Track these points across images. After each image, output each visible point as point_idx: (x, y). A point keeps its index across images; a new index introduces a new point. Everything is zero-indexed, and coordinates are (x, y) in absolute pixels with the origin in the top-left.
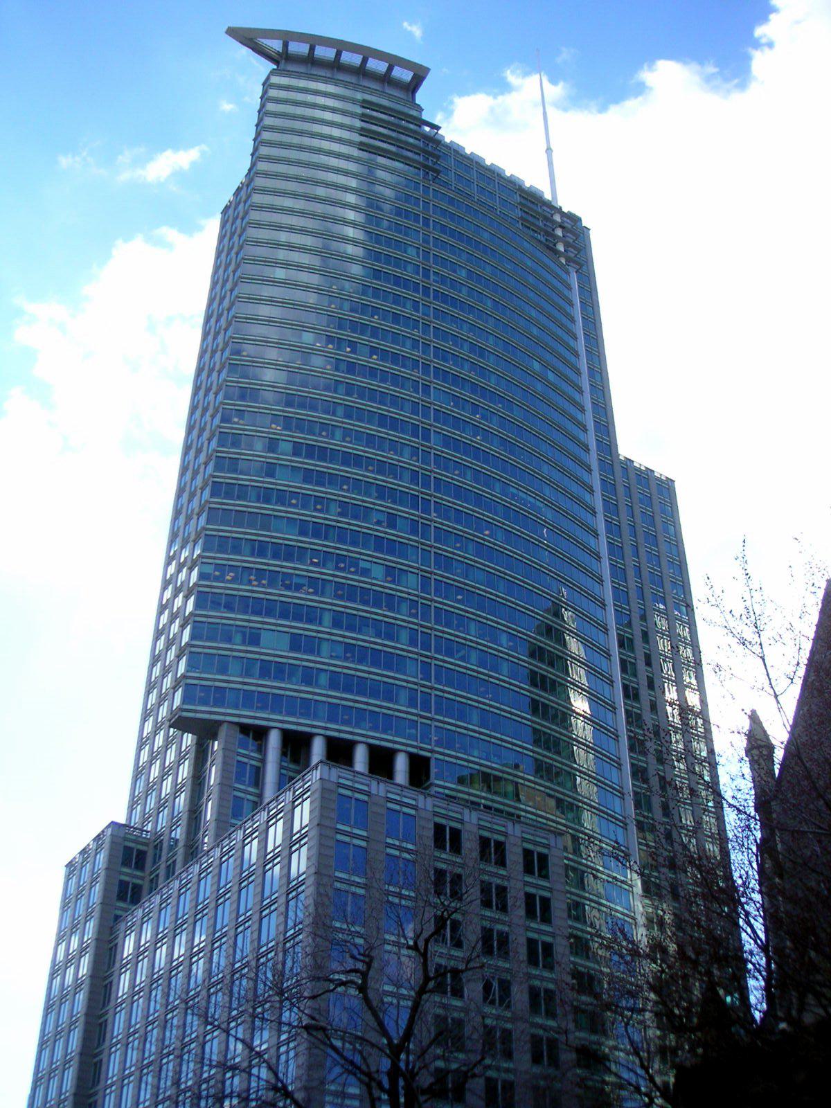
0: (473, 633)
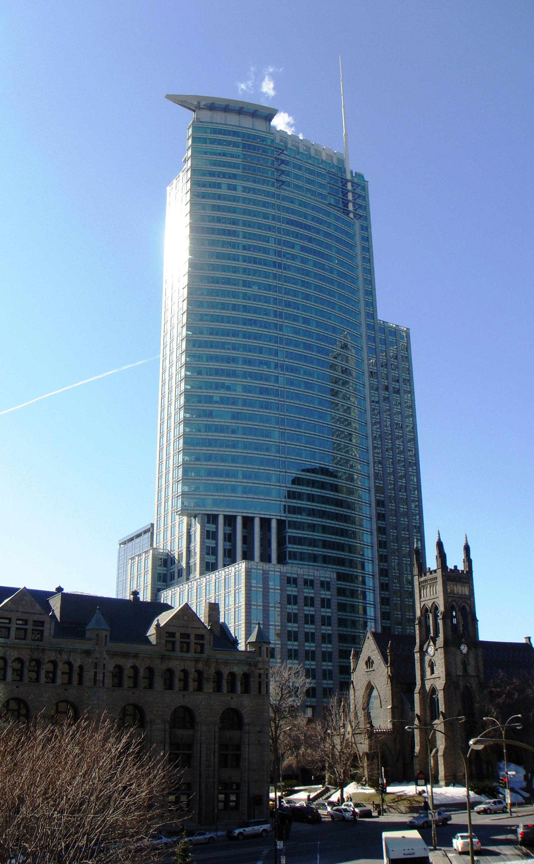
0: (303, 438)
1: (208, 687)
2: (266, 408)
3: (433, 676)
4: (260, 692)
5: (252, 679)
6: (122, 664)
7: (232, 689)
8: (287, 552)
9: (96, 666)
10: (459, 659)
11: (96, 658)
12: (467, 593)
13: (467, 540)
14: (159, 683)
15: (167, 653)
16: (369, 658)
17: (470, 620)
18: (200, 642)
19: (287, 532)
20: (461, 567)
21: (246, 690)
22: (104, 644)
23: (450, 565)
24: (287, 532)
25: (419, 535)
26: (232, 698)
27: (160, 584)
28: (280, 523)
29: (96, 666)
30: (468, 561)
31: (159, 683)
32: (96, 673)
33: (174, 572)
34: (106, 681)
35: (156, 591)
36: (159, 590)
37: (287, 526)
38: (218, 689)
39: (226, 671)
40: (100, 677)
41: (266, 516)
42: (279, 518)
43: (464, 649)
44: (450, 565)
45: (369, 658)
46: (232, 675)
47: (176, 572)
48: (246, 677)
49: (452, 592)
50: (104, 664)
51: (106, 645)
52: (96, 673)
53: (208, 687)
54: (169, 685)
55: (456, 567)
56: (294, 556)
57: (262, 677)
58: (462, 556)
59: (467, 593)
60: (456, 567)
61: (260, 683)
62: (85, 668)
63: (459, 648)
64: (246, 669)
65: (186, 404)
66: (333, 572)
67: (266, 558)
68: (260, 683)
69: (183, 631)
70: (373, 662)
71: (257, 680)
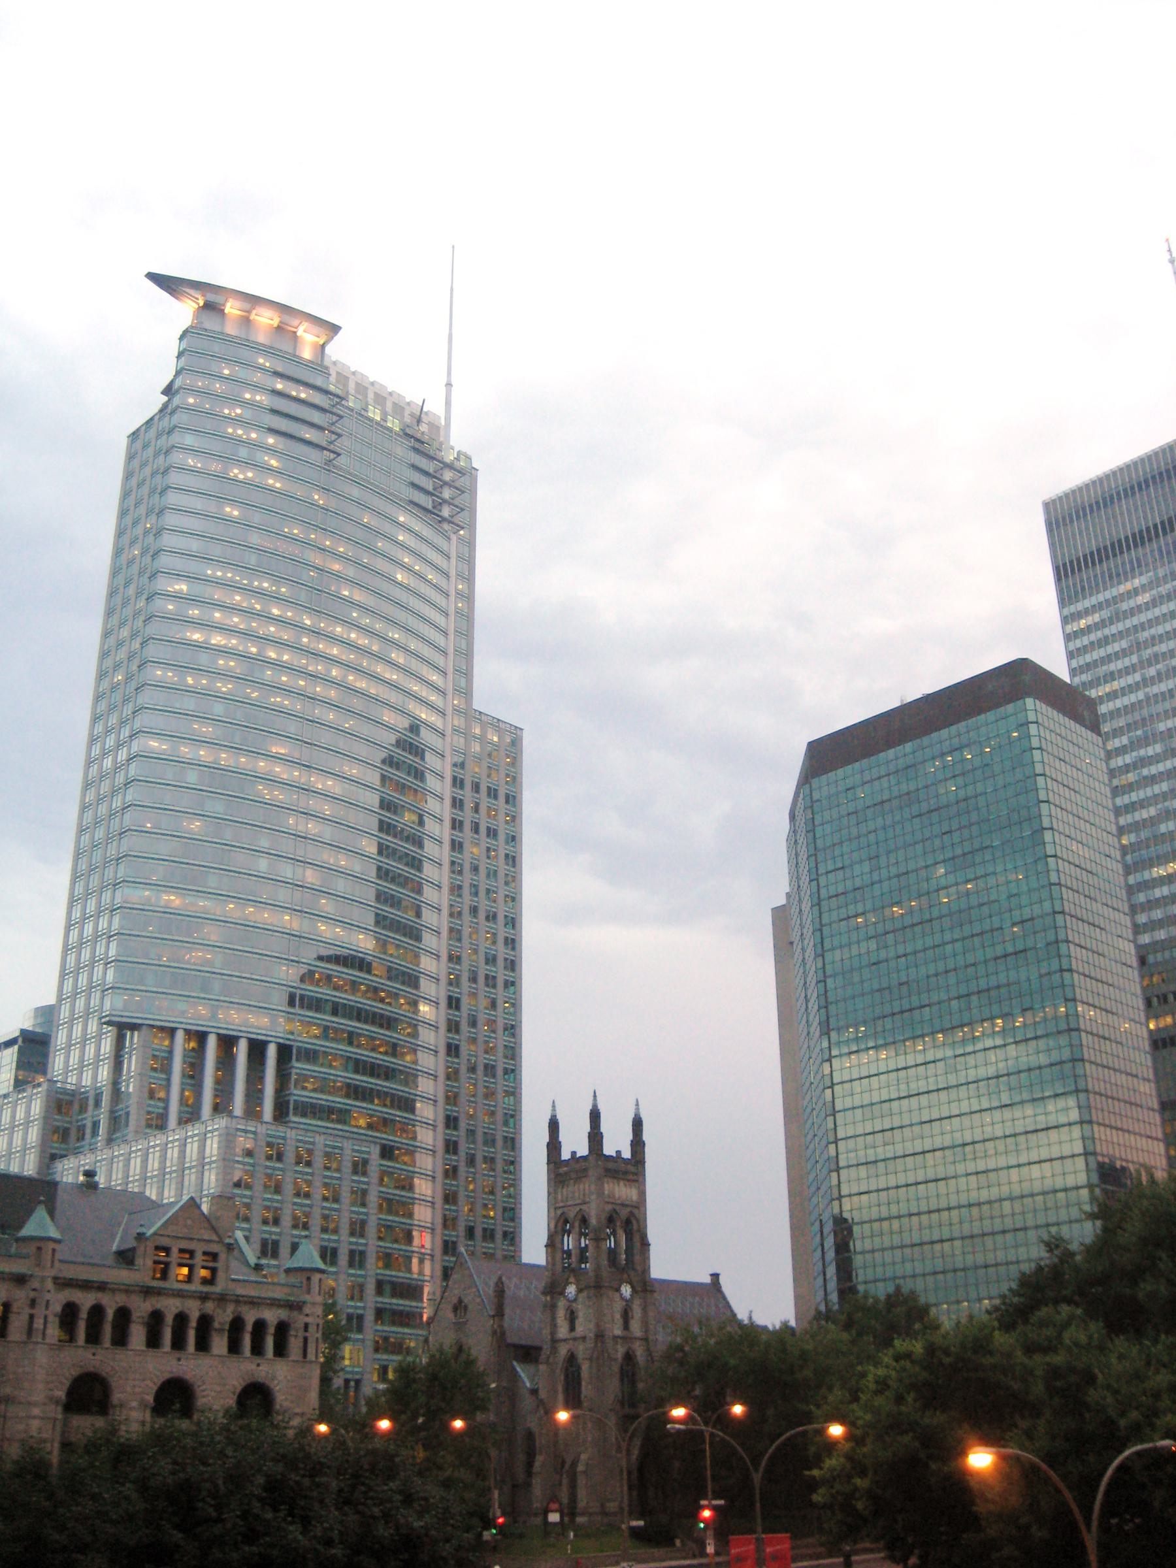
1: (219, 1344)
2: (389, 810)
3: (573, 1334)
4: (305, 1355)
5: (292, 1333)
6: (77, 1301)
7: (257, 1350)
8: (292, 1103)
9: (33, 1303)
10: (618, 1306)
11: (34, 1290)
12: (635, 1198)
13: (637, 1109)
14: (138, 1334)
15: (155, 1284)
16: (460, 1301)
17: (637, 1245)
18: (211, 1264)
19: (292, 1067)
20: (627, 1154)
21: (281, 1350)
22: (49, 1265)
23: (609, 1149)
24: (292, 1067)
25: (164, 1076)
26: (258, 1365)
27: (56, 1147)
28: (284, 1052)
29: (33, 1303)
30: (638, 1143)
31: (138, 1334)
32: (32, 1317)
33: (84, 1126)
34: (49, 1331)
35: (50, 1158)
36: (53, 1157)
37: (294, 1057)
38: (234, 1347)
39: (250, 1317)
40: (38, 1324)
41: (260, 1037)
42: (281, 1041)
43: (626, 1290)
44: (609, 1149)
45: (460, 1301)
46: (260, 1326)
47: (89, 1125)
48: (282, 1329)
49: (612, 1195)
50: (48, 1301)
51: (52, 1266)
52: (32, 1317)
53: (219, 1344)
54: (153, 1341)
55: (618, 1152)
56: (308, 1110)
57: (310, 1329)
58: (629, 1136)
59: (635, 1198)
60: (618, 1152)
61: (306, 1340)
62: (15, 1308)
63: (618, 1290)
64: (283, 1314)
65: (1066, 612)
66: (375, 1143)
67: (252, 1110)
68: (306, 1340)
69: (184, 1245)
70: (466, 1308)
71: (301, 1334)
